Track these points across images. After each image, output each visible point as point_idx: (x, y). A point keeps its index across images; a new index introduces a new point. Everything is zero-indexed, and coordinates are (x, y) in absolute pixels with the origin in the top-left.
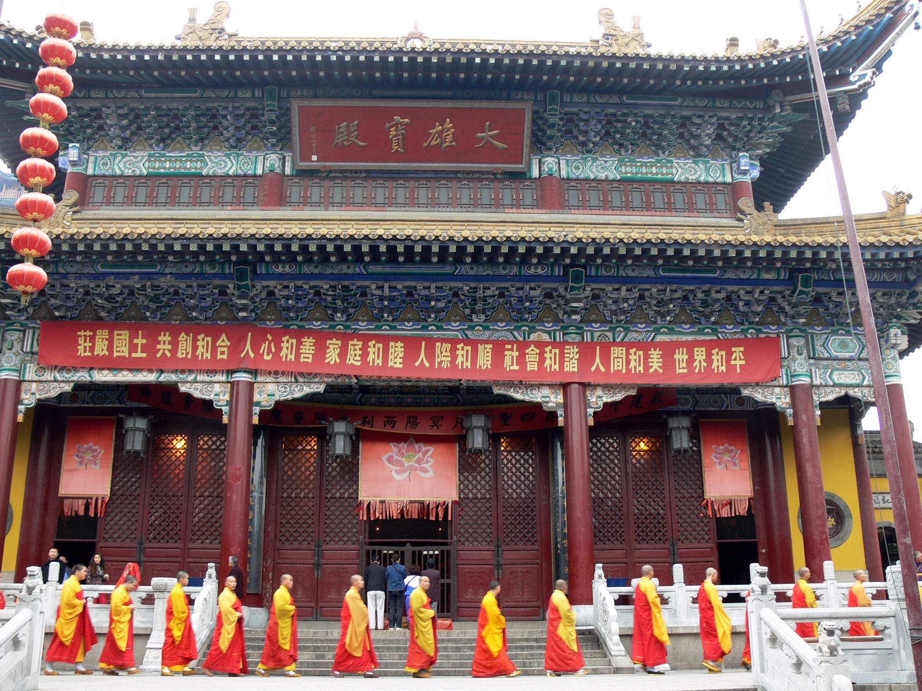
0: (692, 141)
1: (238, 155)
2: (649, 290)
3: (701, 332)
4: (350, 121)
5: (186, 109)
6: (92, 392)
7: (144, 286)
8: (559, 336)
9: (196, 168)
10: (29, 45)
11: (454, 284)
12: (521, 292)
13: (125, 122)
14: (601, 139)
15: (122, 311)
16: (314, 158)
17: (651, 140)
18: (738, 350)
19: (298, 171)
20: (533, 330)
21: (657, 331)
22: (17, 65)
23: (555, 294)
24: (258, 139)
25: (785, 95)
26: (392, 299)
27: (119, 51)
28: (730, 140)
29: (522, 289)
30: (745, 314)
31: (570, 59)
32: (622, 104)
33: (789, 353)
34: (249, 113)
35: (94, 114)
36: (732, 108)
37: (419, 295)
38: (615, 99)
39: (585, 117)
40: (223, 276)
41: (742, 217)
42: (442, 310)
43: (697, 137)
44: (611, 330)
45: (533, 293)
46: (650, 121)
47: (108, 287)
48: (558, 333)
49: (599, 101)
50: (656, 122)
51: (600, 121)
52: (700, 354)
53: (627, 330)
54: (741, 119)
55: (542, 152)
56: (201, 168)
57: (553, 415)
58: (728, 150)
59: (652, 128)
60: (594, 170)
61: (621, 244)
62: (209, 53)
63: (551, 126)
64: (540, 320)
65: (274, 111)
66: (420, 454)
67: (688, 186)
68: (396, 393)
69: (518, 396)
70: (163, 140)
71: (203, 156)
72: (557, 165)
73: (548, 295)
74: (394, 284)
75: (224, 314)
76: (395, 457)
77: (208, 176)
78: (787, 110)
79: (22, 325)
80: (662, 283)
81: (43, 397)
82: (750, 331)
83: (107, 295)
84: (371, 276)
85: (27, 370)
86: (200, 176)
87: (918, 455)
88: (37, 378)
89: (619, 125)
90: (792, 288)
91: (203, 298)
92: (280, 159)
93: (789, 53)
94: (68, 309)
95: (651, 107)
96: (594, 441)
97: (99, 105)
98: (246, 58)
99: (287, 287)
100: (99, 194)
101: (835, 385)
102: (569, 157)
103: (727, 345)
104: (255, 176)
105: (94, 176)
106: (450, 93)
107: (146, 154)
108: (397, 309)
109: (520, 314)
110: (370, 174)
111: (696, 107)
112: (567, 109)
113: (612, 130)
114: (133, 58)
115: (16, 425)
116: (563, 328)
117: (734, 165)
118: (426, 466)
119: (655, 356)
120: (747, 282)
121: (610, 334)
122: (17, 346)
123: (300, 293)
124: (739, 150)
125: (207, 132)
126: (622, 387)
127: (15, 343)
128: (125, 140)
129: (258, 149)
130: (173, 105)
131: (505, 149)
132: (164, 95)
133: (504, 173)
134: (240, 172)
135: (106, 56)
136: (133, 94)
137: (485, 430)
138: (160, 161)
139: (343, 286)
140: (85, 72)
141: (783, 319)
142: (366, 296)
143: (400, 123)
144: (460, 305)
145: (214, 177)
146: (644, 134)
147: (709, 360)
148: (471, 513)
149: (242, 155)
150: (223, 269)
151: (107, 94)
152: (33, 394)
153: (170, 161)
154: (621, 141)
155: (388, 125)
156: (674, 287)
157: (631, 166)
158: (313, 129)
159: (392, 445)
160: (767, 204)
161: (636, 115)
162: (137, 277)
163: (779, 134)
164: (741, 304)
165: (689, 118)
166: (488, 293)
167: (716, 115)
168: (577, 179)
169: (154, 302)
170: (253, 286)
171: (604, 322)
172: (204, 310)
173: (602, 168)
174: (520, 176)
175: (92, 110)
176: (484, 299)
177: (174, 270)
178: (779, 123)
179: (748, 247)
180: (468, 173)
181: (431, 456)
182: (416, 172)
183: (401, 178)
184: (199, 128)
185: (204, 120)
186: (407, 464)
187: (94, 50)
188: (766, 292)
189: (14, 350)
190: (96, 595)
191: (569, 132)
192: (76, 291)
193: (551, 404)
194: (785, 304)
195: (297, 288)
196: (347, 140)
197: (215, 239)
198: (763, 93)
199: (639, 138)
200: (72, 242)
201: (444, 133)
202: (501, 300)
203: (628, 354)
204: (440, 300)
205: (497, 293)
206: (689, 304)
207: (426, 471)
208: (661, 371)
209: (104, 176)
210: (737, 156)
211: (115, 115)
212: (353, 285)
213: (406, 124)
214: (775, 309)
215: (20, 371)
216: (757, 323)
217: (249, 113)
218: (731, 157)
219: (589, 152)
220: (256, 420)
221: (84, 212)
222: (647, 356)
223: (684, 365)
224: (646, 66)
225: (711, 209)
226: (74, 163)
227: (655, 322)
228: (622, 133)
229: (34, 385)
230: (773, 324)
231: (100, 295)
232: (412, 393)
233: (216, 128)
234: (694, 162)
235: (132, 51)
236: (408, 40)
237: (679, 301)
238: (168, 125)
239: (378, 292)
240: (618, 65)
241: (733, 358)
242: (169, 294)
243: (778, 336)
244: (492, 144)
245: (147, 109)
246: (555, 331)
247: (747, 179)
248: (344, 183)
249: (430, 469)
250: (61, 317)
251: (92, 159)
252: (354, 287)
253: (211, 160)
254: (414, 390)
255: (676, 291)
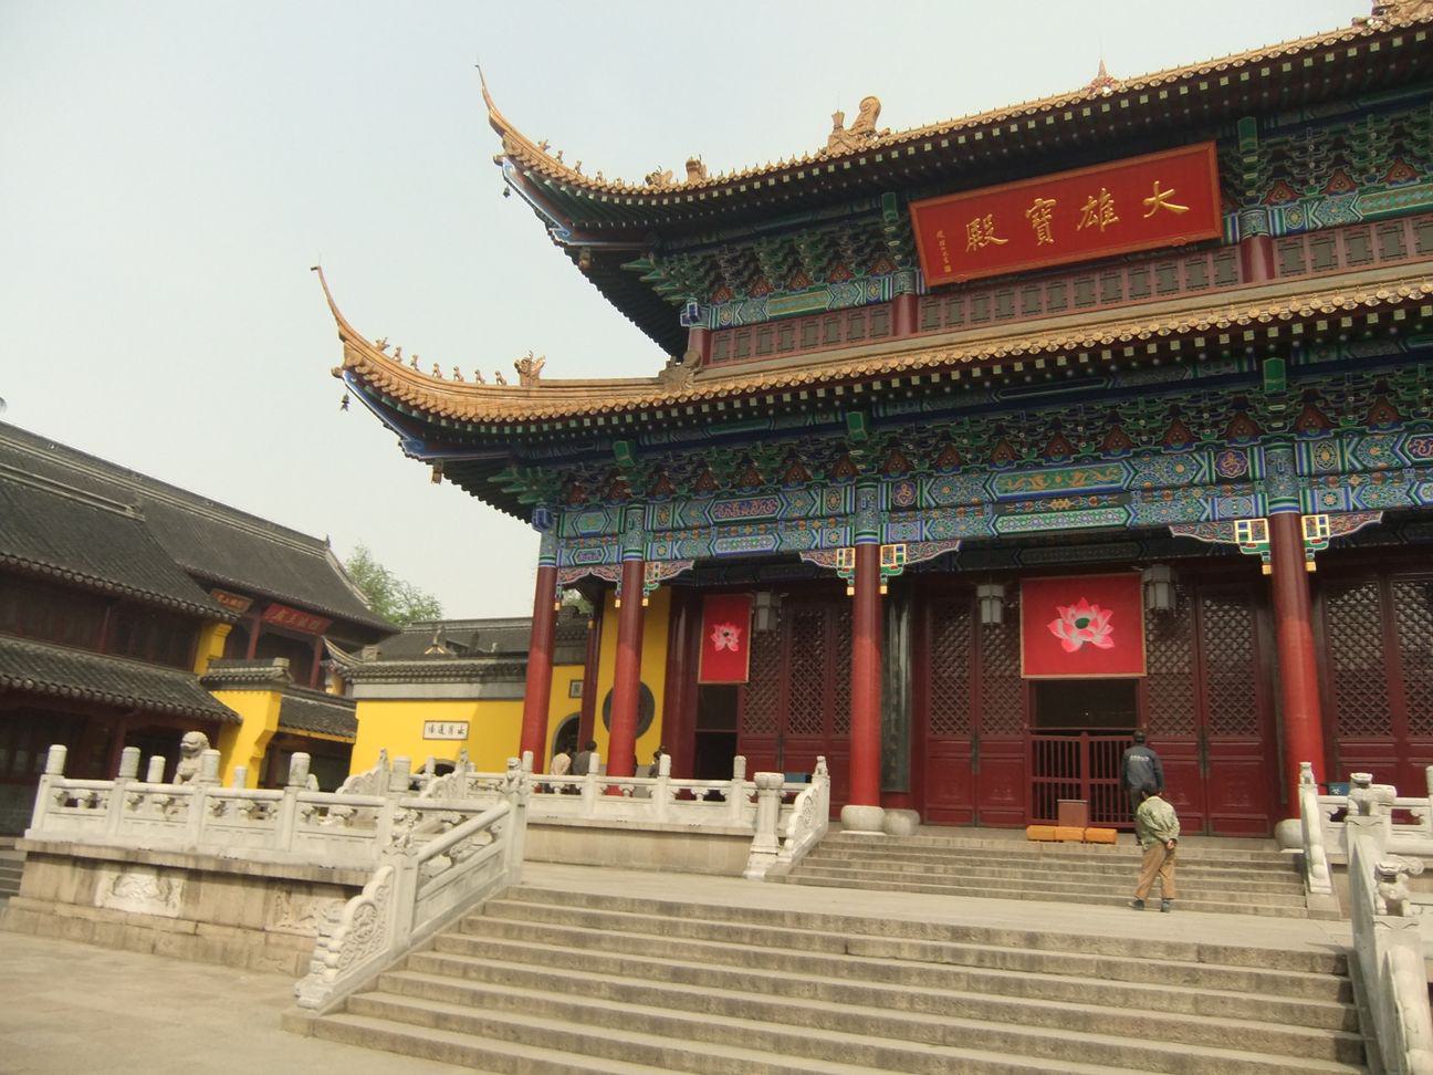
16: (948, 269)
19: (932, 288)
48: (1256, 449)
57: (1256, 561)
98: (863, 161)
99: (962, 423)
101: (577, 566)
115: (642, 611)
131: (1186, 213)
160: (514, 380)
190: (705, 791)
191: (1340, 161)
196: (983, 241)
236: (1092, 90)
246: (1252, 447)
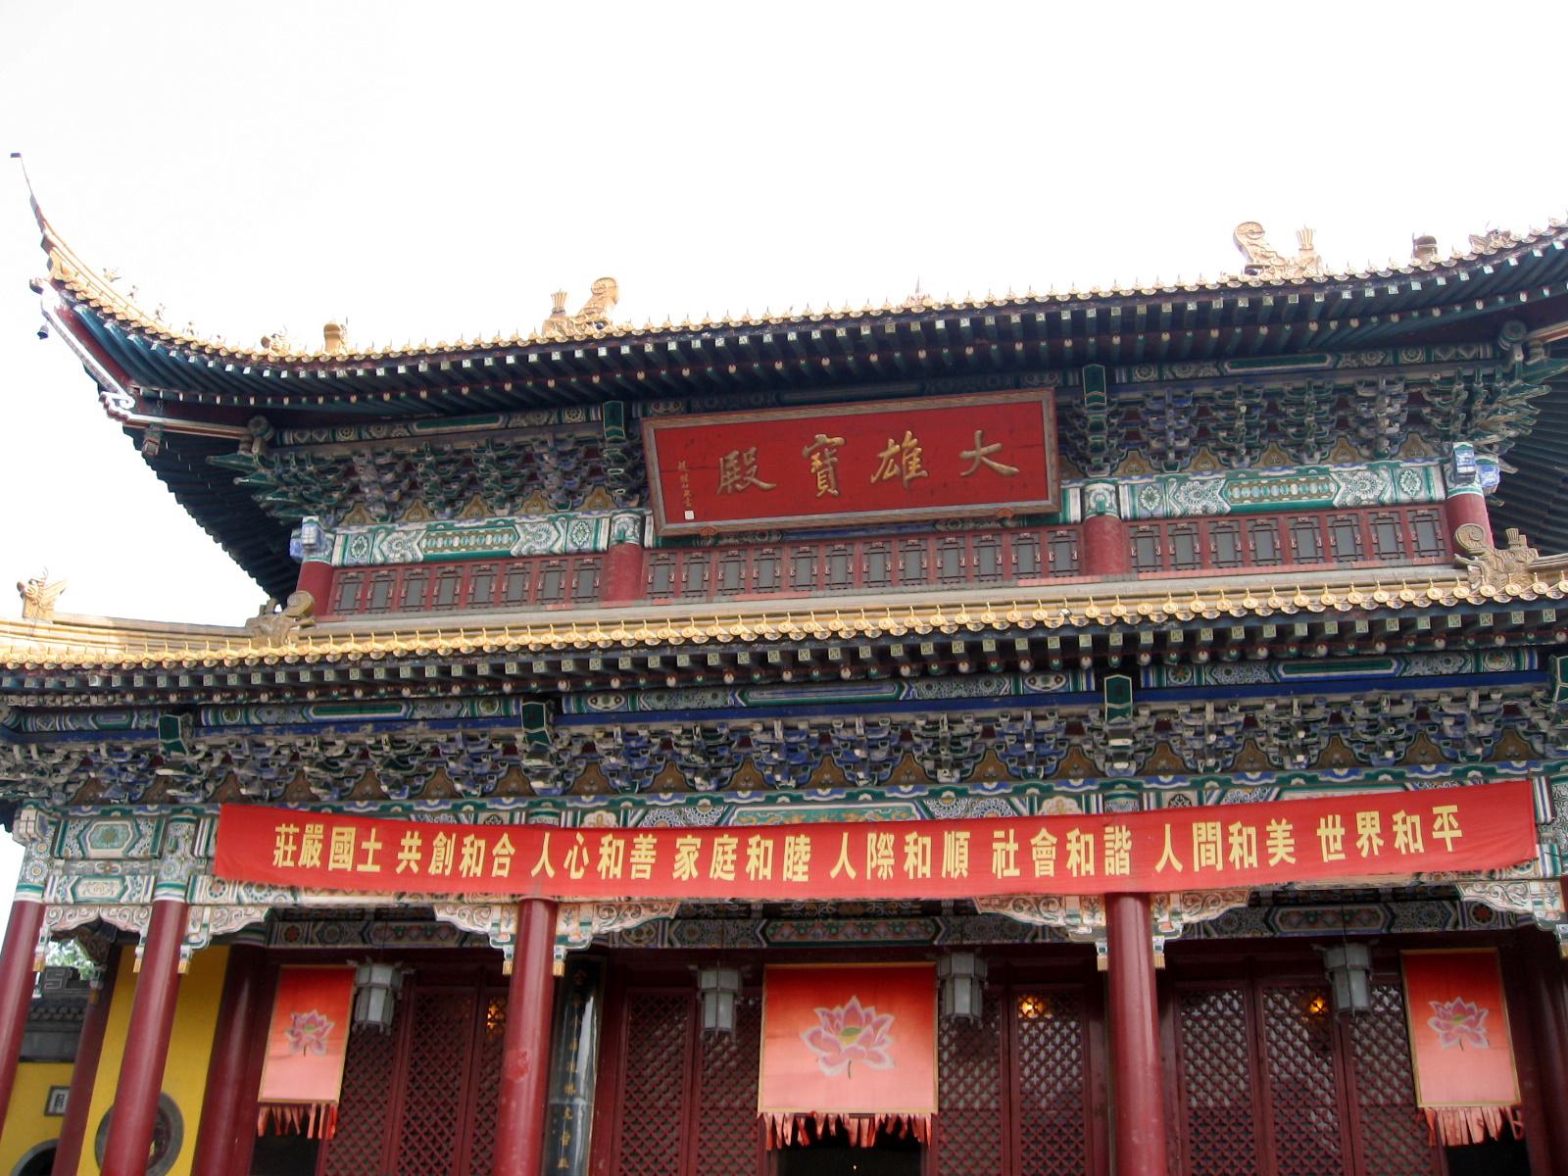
0: (1363, 431)
1: (569, 519)
2: (1261, 707)
3: (1371, 780)
4: (743, 449)
5: (481, 449)
6: (321, 924)
7: (379, 742)
8: (1096, 804)
9: (501, 545)
10: (229, 368)
11: (898, 717)
12: (1019, 726)
13: (389, 477)
14: (1193, 442)
15: (422, 783)
16: (689, 515)
17: (1285, 436)
18: (1445, 812)
20: (1047, 793)
21: (1285, 784)
22: (218, 401)
23: (1085, 725)
24: (603, 490)
25: (1530, 328)
26: (791, 750)
27: (359, 363)
28: (1436, 421)
29: (1020, 719)
30: (1457, 742)
31: (1102, 306)
32: (1223, 379)
33: (1554, 813)
34: (583, 449)
35: (341, 467)
36: (1430, 363)
37: (839, 740)
38: (1210, 370)
39: (1156, 407)
40: (507, 720)
41: (1465, 560)
42: (884, 764)
43: (1371, 423)
44: (1195, 785)
45: (1041, 726)
46: (1279, 401)
47: (324, 745)
48: (1093, 798)
49: (1180, 375)
50: (1289, 403)
51: (1186, 411)
52: (1368, 824)
53: (1225, 785)
54: (1450, 381)
55: (1086, 476)
56: (509, 544)
57: (1089, 950)
58: (1437, 441)
59: (1284, 415)
60: (1181, 498)
61: (1174, 624)
62: (498, 354)
63: (1097, 428)
64: (1062, 775)
65: (619, 441)
66: (869, 1028)
67: (1362, 512)
68: (826, 917)
69: (1023, 917)
70: (451, 502)
71: (512, 524)
72: (1113, 495)
73: (1074, 729)
74: (792, 721)
75: (514, 785)
76: (824, 1034)
77: (520, 557)
78: (1537, 354)
79: (195, 812)
80: (1285, 694)
81: (220, 931)
82: (1471, 774)
83: (322, 758)
84: (754, 711)
85: (198, 885)
86: (507, 557)
87: (551, 1079)
88: (211, 900)
89: (1222, 414)
90: (1547, 685)
91: (476, 759)
92: (635, 522)
93: (1514, 250)
94: (267, 784)
95: (1278, 376)
96: (1377, 993)
97: (348, 453)
100: (348, 594)
102: (1136, 480)
103: (1422, 805)
104: (596, 552)
105: (343, 567)
106: (914, 387)
107: (424, 526)
108: (805, 765)
109: (1035, 766)
110: (787, 538)
111: (1362, 368)
112: (1123, 396)
113: (1211, 425)
114: (380, 372)
116: (1103, 787)
117: (1447, 466)
118: (880, 1049)
119: (1280, 834)
120: (1456, 679)
121: (1192, 795)
122: (184, 848)
123: (633, 744)
124: (1455, 439)
125: (517, 484)
126: (1225, 896)
127: (181, 842)
128: (392, 506)
129: (603, 507)
130: (460, 445)
131: (1013, 475)
132: (447, 429)
133: (1016, 517)
134: (571, 547)
135: (341, 373)
136: (399, 431)
137: (976, 981)
138: (444, 536)
139: (704, 730)
140: (300, 401)
141: (1538, 747)
142: (750, 745)
143: (829, 446)
144: (917, 754)
145: (529, 558)
146: (1272, 427)
147: (1387, 832)
148: (960, 1138)
149: (575, 518)
150: (506, 708)
151: (360, 435)
152: (205, 926)
153: (461, 536)
154: (1230, 444)
155: (806, 450)
156: (1309, 699)
157: (1250, 486)
158: (682, 465)
159: (818, 1011)
160: (1512, 532)
161: (1248, 394)
162: (370, 727)
163: (1529, 401)
164: (1448, 723)
165: (1351, 390)
166: (959, 730)
167: (1401, 379)
168: (1152, 518)
169: (397, 768)
170: (557, 736)
171: (1181, 772)
172: (479, 779)
173: (1197, 495)
174: (1044, 522)
175: (339, 461)
176: (955, 742)
177: (428, 714)
178: (1526, 380)
179: (1421, 611)
180: (954, 522)
181: (890, 1032)
182: (863, 527)
183: (841, 540)
184: (504, 478)
185: (511, 464)
186: (845, 1046)
187: (323, 365)
188: (1496, 696)
189: (179, 853)
191: (1133, 435)
192: (278, 753)
193: (1082, 930)
194: (1537, 718)
195: (628, 736)
197: (464, 656)
198: (1486, 329)
199: (1262, 436)
200: (244, 671)
201: (903, 456)
202: (990, 742)
203: (1226, 834)
204: (876, 747)
205: (979, 728)
206: (1345, 729)
207: (879, 1059)
208: (1292, 860)
209: (357, 566)
210: (1451, 447)
211: (371, 467)
212: (722, 726)
213: (837, 447)
214: (1522, 728)
215: (188, 888)
216: (1486, 759)
217: (583, 449)
218: (1442, 454)
219: (1172, 467)
220: (558, 969)
221: (318, 626)
222: (1263, 836)
223: (1339, 846)
224: (1243, 303)
225: (1407, 551)
226: (311, 549)
227: (1281, 768)
228: (1230, 429)
229: (208, 911)
230: (1518, 759)
231: (311, 760)
232: (856, 917)
233: (533, 477)
234: (1371, 468)
235: (377, 363)
237: (1325, 725)
238: (456, 478)
239: (766, 738)
240: (1191, 307)
241: (1437, 825)
242: (423, 753)
243: (1529, 780)
244: (992, 469)
245: (420, 454)
246: (1087, 794)
247: (1476, 489)
248: (742, 554)
249: (886, 1056)
250: (255, 797)
251: (340, 540)
252: (725, 731)
253: (525, 530)
254: (860, 910)
255: (1313, 706)
